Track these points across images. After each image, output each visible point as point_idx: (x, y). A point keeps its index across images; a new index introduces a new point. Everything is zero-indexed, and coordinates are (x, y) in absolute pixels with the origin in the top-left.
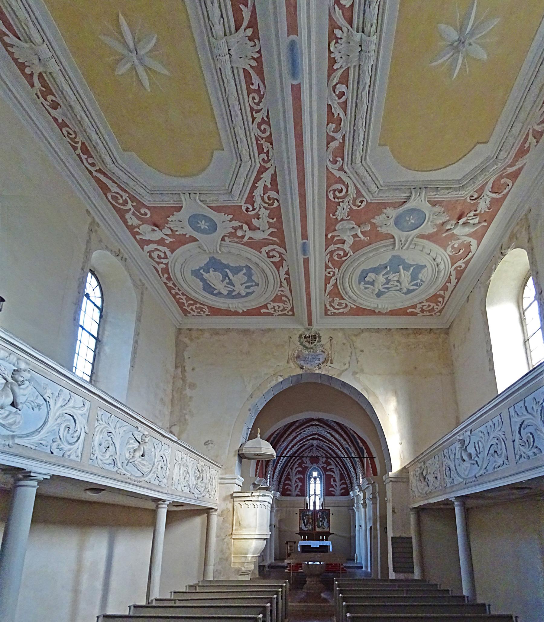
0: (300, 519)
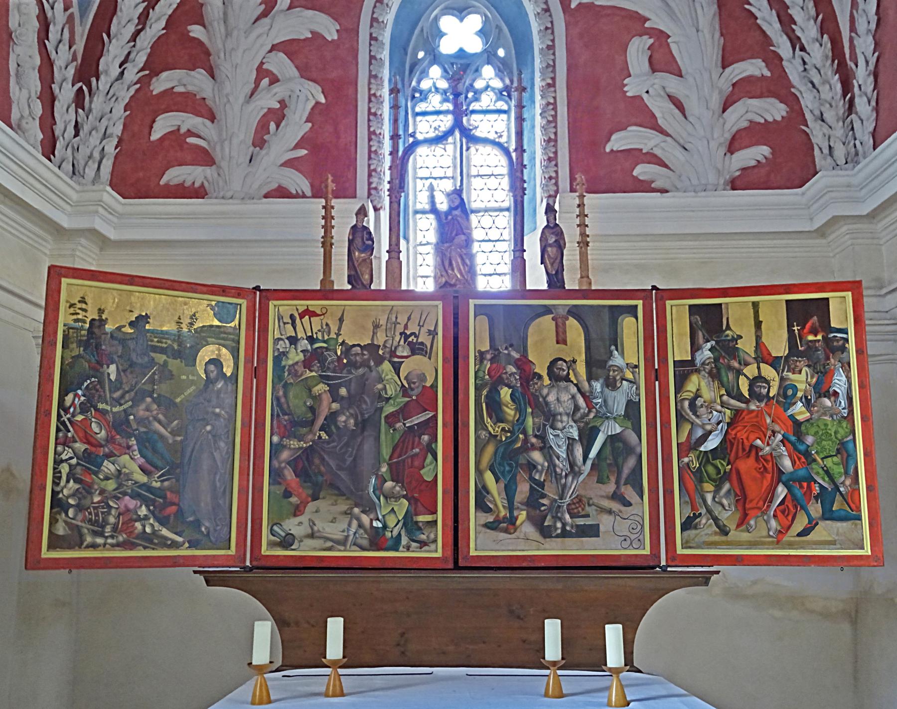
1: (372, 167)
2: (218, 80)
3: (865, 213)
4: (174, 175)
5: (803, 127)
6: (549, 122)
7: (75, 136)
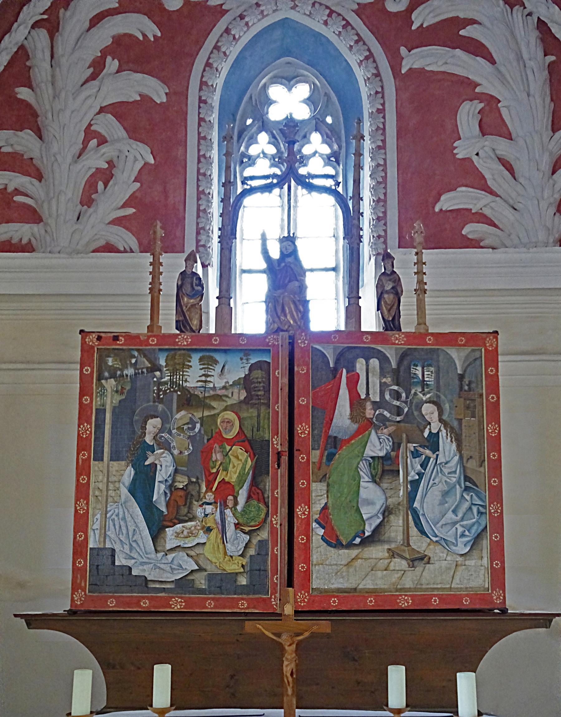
0: (88, 449)
1: (200, 226)
6: (379, 183)
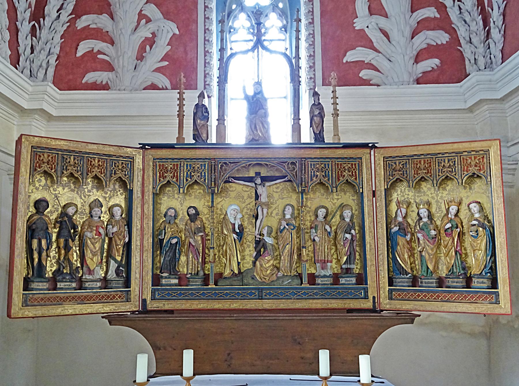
1: (206, 72)
2: (116, 20)
3: (499, 98)
4: (90, 77)
5: (459, 48)
7: (31, 54)
